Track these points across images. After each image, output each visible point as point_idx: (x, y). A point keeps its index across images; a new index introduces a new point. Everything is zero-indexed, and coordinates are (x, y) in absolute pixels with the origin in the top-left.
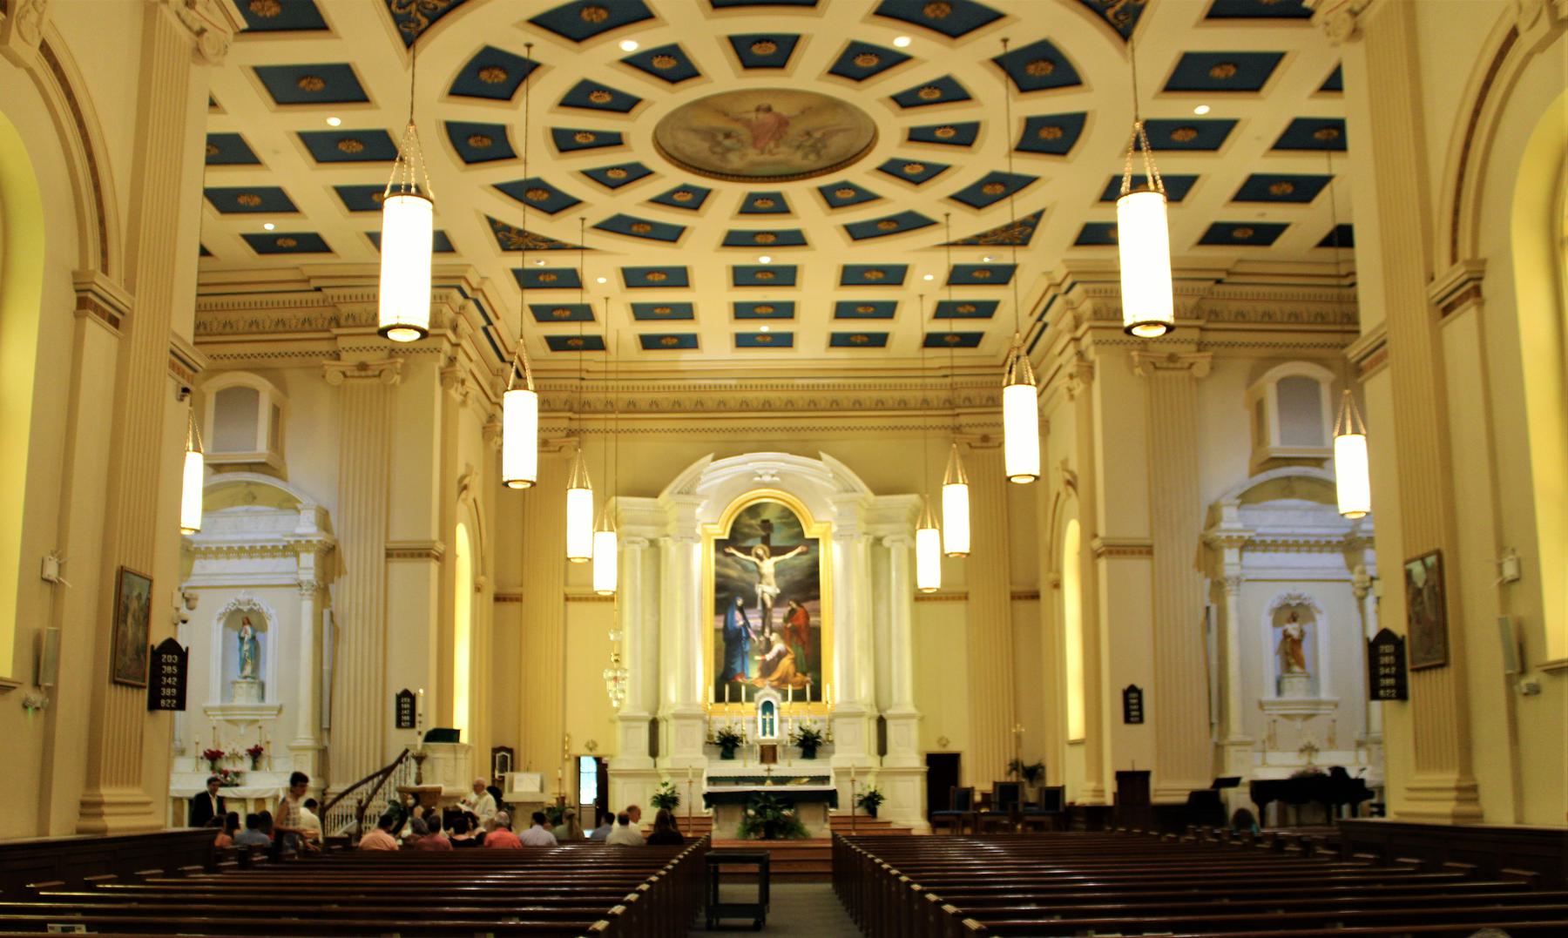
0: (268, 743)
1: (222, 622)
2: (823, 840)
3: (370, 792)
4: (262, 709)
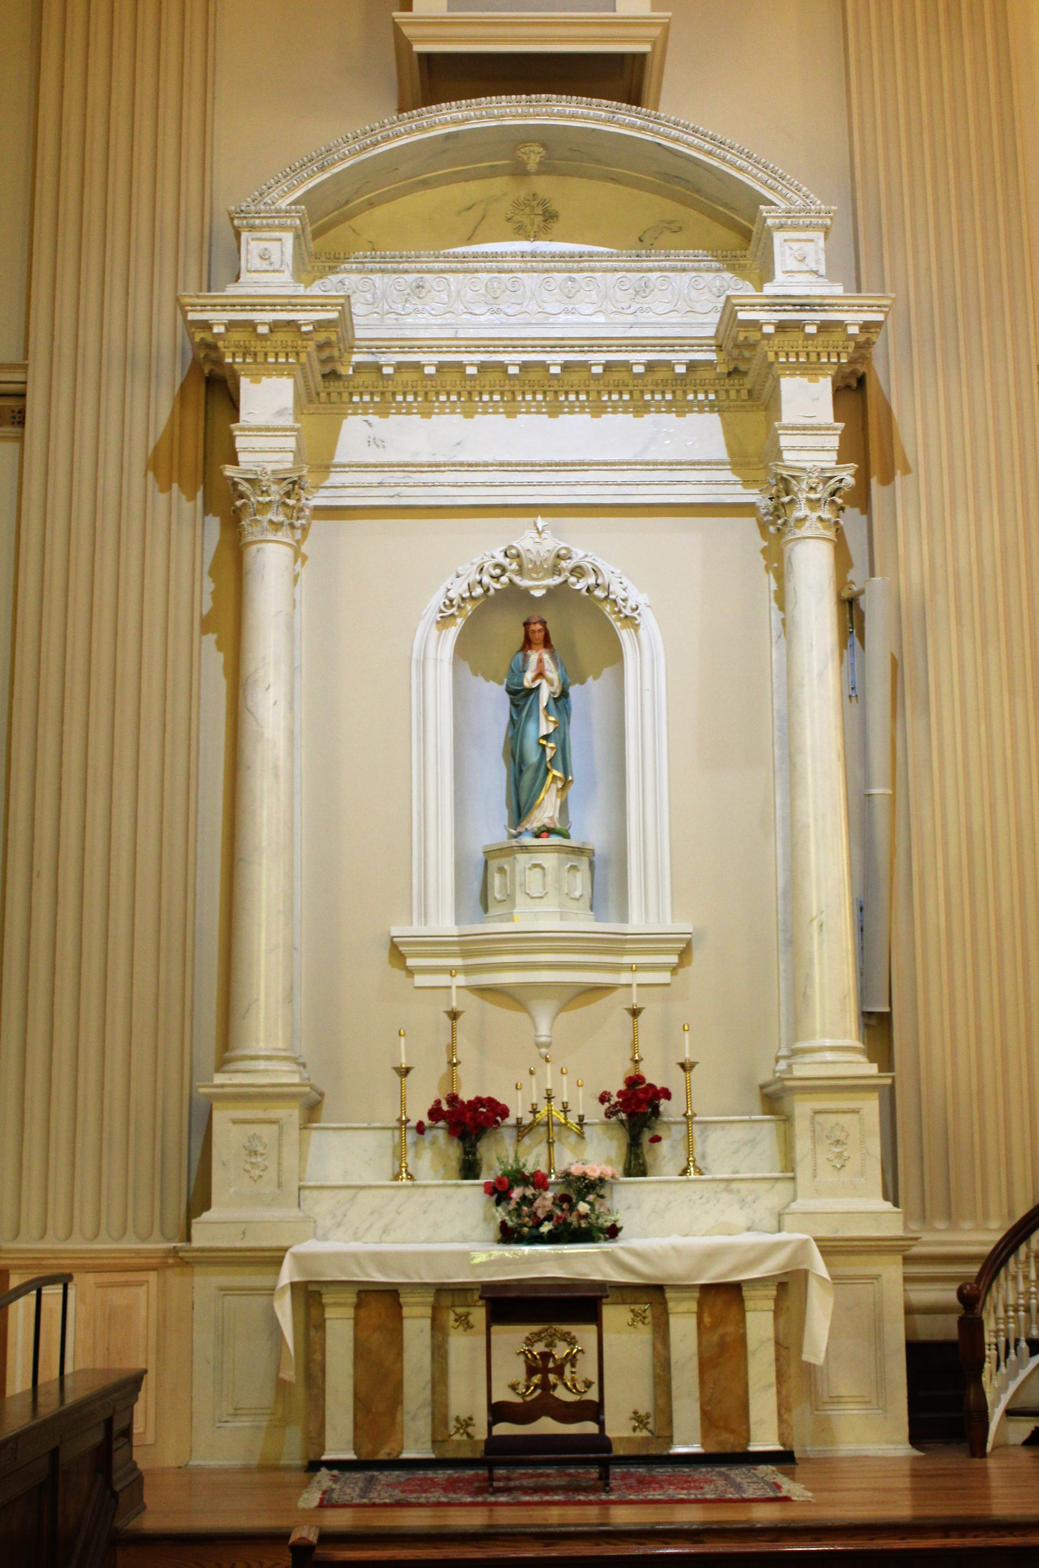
0: (685, 1067)
1: (453, 632)
2: (336, 1304)
3: (1012, 1260)
4: (616, 944)
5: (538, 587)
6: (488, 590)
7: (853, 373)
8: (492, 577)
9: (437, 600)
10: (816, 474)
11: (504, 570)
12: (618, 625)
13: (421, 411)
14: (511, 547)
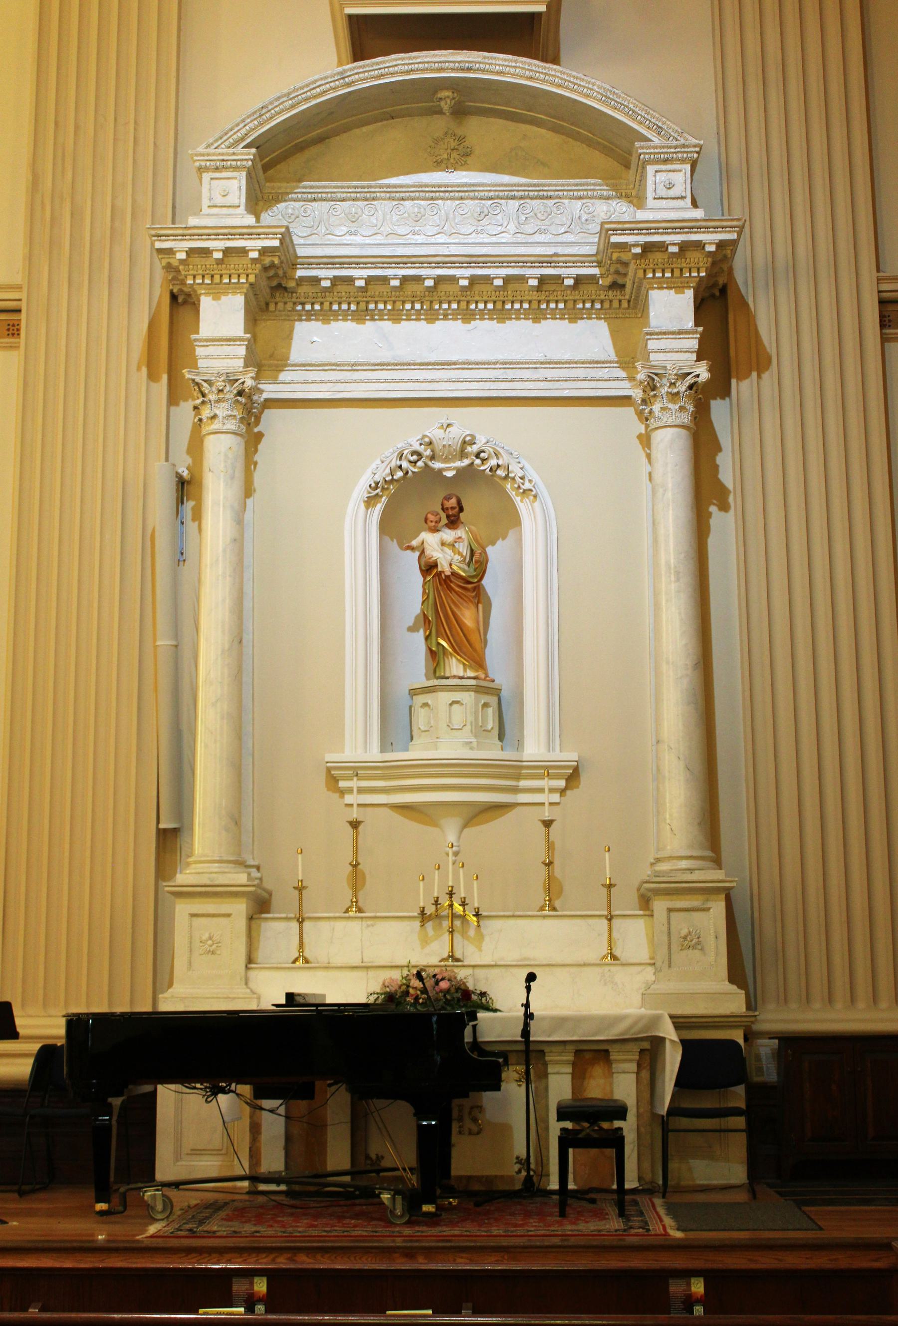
1: (379, 507)
5: (449, 469)
6: (407, 473)
7: (715, 285)
8: (410, 462)
9: (365, 481)
10: (222, 379)
11: (419, 455)
12: (517, 500)
13: (390, 317)
14: (424, 436)
